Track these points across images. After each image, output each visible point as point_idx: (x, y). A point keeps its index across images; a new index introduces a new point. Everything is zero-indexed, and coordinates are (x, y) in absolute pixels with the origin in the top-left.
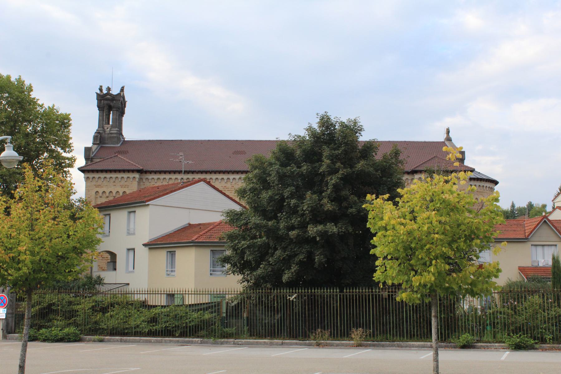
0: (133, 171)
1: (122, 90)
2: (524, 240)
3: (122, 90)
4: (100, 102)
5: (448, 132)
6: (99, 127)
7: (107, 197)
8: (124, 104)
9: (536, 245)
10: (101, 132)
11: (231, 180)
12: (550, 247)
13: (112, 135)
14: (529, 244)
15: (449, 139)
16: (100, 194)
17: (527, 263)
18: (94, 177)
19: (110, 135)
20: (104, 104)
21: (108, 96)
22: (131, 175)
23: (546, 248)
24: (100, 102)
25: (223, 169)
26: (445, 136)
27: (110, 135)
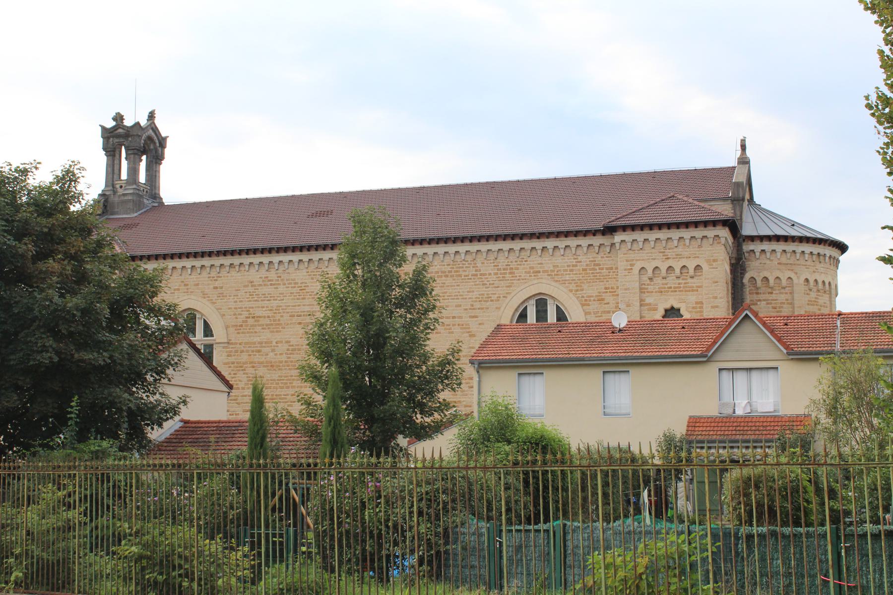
0: (714, 223)
1: (152, 116)
2: (702, 359)
3: (152, 116)
4: (108, 141)
5: (743, 147)
6: (106, 186)
7: (678, 278)
8: (162, 142)
9: (733, 370)
10: (107, 193)
11: (276, 265)
12: (764, 373)
13: (126, 198)
14: (713, 368)
15: (744, 161)
16: (691, 271)
17: (709, 409)
18: (203, 266)
19: (123, 198)
20: (113, 144)
21: (120, 130)
22: (711, 232)
23: (755, 375)
24: (108, 141)
25: (275, 244)
26: (739, 153)
27: (123, 198)
